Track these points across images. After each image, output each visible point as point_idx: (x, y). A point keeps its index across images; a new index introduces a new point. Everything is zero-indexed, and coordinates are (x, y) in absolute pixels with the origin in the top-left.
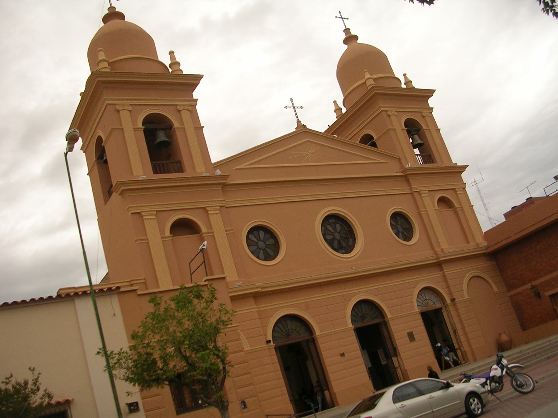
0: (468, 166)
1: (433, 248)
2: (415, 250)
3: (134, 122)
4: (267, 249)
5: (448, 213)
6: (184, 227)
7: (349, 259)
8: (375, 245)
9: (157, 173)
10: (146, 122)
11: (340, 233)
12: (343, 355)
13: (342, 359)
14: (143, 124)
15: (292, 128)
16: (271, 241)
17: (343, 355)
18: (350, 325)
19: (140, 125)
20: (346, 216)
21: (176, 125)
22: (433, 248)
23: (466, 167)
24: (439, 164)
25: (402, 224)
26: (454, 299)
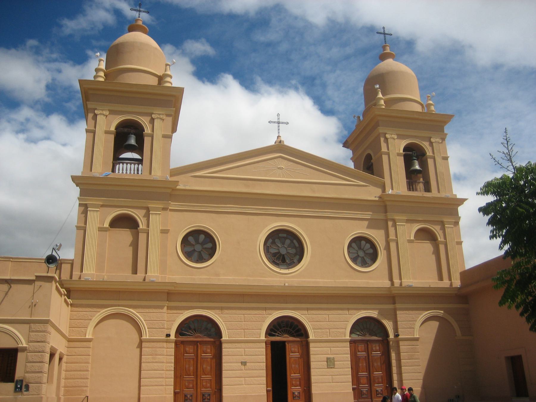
0: (466, 199)
1: (391, 279)
2: (374, 277)
3: (109, 124)
4: (365, 258)
5: (427, 246)
6: (124, 222)
7: (293, 274)
8: (324, 264)
9: (410, 190)
10: (406, 149)
11: (285, 248)
12: (244, 363)
13: (243, 367)
14: (404, 151)
15: (271, 141)
16: (371, 251)
17: (244, 363)
18: (263, 337)
19: (113, 129)
20: (206, 230)
21: (429, 153)
22: (391, 279)
23: (465, 200)
24: (434, 193)
25: (363, 251)
26: (398, 335)
